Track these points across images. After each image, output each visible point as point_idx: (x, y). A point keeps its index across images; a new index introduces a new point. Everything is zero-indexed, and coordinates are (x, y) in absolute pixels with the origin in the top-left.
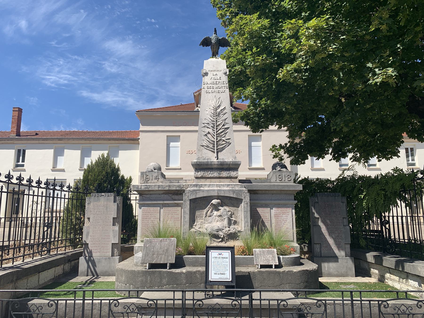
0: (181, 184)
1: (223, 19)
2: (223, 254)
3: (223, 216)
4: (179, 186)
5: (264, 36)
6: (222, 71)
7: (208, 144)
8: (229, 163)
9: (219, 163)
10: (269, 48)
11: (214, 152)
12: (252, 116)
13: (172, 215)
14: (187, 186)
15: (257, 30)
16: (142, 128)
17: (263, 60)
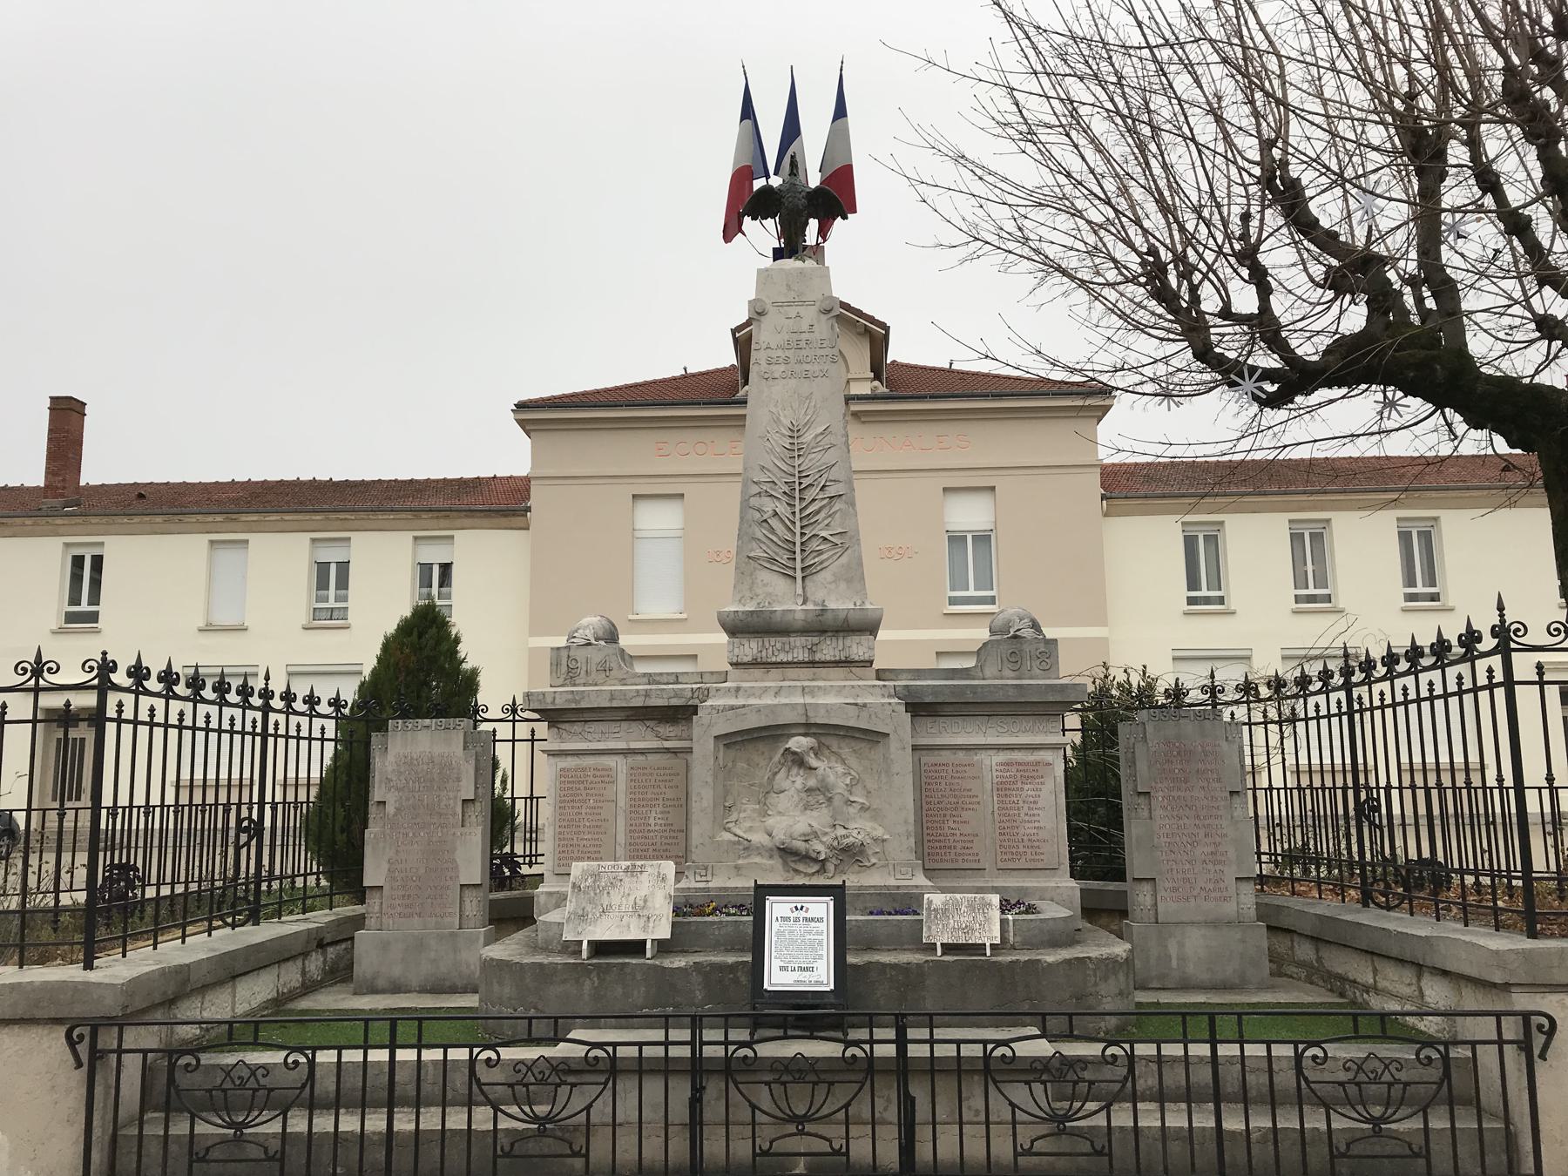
2: (808, 909)
6: (818, 304)
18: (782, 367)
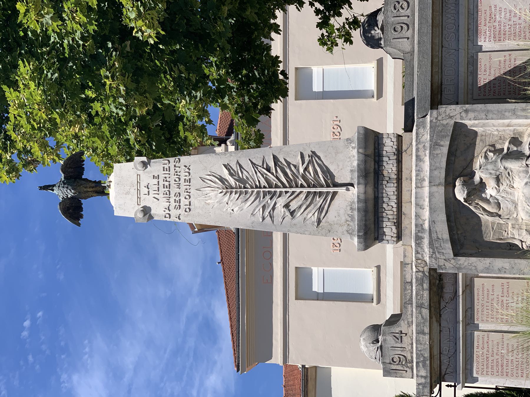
0: (414, 277)
1: (21, 166)
3: (498, 173)
4: (420, 282)
5: (56, 75)
6: (139, 173)
7: (313, 209)
8: (362, 157)
9: (362, 181)
10: (84, 61)
11: (335, 194)
12: (246, 98)
13: (496, 299)
14: (419, 261)
15: (44, 91)
16: (277, 358)
17: (113, 77)
18: (182, 199)
